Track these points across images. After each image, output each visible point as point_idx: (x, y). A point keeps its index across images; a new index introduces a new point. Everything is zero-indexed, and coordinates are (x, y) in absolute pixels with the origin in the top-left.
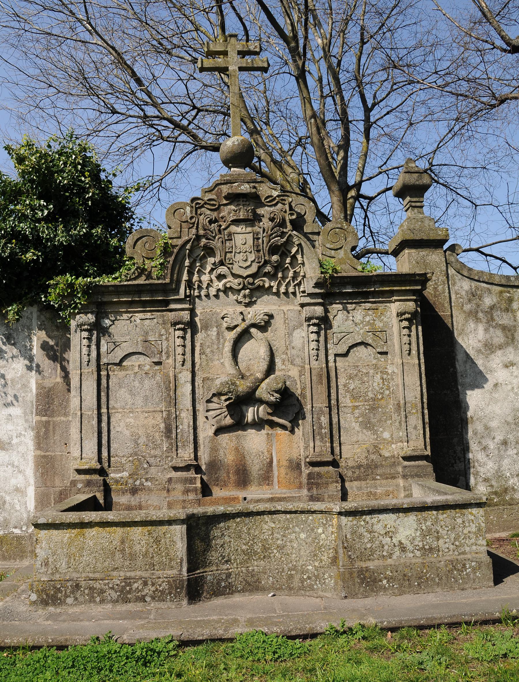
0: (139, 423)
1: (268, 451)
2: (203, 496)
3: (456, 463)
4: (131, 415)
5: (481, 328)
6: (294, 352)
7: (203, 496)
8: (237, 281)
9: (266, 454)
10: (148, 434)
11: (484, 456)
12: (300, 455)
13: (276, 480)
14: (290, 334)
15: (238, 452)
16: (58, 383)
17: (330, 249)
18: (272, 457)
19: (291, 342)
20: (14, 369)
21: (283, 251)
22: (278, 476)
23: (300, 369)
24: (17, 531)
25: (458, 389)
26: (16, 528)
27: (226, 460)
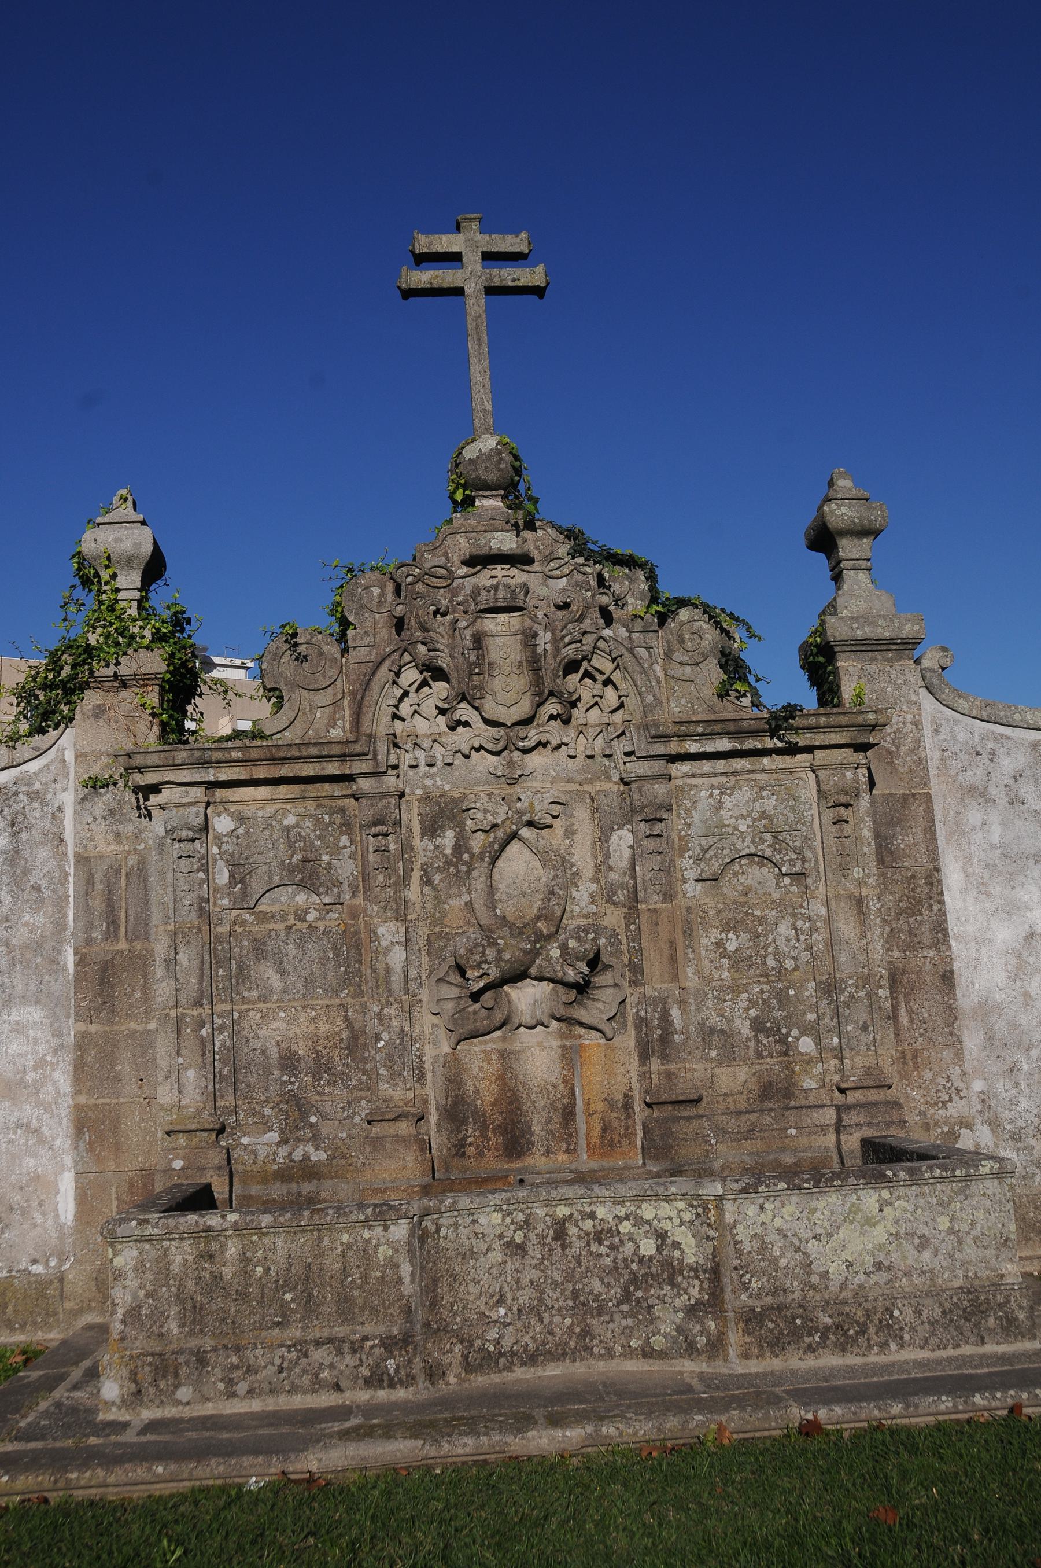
0: (298, 1031)
1: (565, 1082)
2: (483, 253)
3: (950, 1100)
4: (282, 1014)
5: (994, 818)
6: (614, 877)
7: (483, 253)
8: (493, 731)
9: (561, 1087)
10: (317, 1052)
11: (1009, 1085)
12: (631, 1089)
13: (582, 1142)
14: (603, 838)
15: (505, 1084)
16: (122, 952)
17: (681, 663)
18: (573, 1094)
19: (607, 856)
20: (27, 924)
21: (586, 670)
22: (587, 1134)
23: (626, 910)
24: (38, 1269)
25: (949, 948)
26: (35, 1262)
27: (479, 1102)
